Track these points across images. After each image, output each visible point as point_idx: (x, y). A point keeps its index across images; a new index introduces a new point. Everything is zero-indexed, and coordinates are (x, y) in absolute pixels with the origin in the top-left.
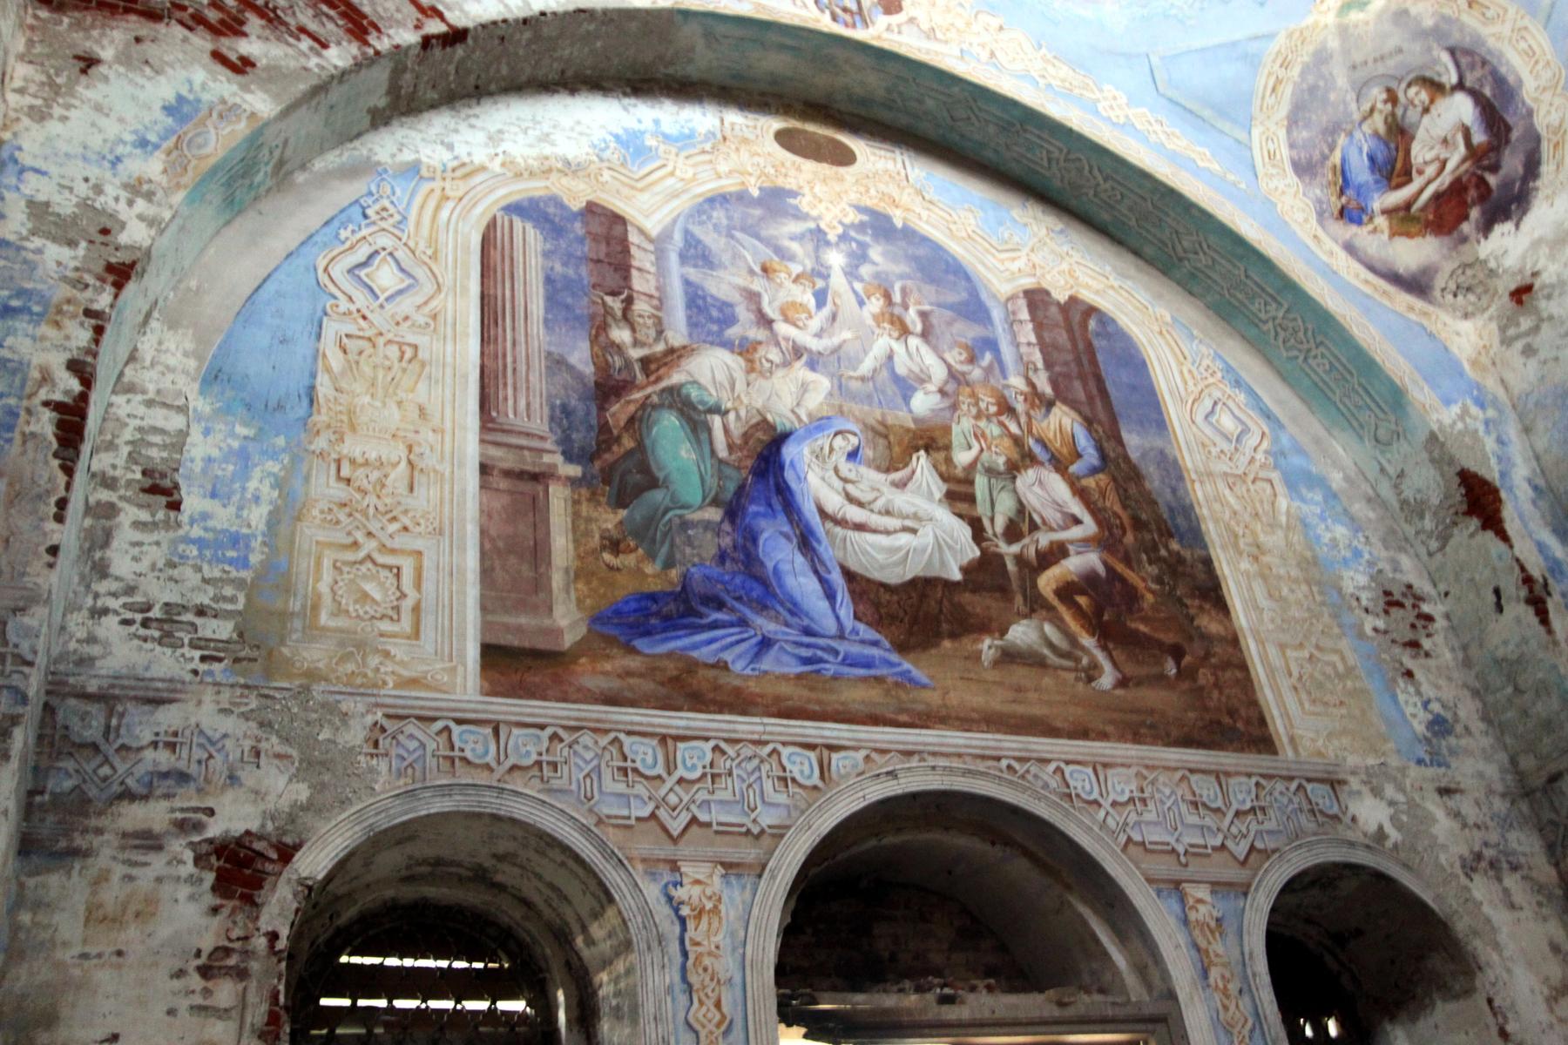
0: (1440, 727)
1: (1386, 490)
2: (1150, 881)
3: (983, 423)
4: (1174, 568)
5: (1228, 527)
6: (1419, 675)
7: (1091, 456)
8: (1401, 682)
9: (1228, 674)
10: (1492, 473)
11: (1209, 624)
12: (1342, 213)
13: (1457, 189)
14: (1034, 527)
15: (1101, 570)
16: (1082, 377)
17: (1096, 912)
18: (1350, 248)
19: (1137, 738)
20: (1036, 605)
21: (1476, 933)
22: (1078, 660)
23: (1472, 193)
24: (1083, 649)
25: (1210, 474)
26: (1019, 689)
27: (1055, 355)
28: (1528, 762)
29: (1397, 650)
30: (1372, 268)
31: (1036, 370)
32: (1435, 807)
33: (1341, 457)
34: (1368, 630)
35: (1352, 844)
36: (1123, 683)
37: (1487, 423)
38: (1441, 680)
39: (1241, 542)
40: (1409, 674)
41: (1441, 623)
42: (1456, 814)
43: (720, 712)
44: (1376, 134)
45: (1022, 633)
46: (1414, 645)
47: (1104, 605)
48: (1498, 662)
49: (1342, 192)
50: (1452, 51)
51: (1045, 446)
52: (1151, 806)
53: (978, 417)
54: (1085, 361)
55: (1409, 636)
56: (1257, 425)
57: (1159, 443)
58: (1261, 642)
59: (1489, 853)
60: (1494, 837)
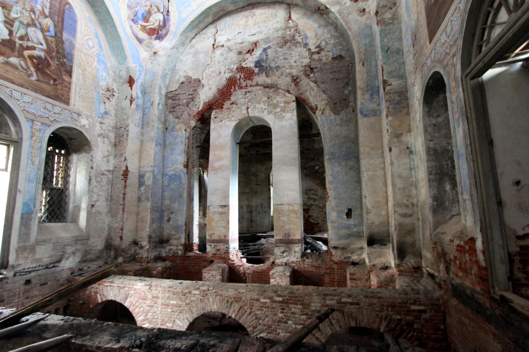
0: (106, 113)
1: (117, 72)
2: (26, 118)
3: (24, 11)
4: (63, 64)
5: (80, 62)
6: (107, 104)
7: (52, 33)
8: (102, 103)
9: (65, 89)
10: (135, 78)
11: (66, 78)
12: (133, 20)
13: (154, 30)
14: (28, 40)
15: (43, 57)
16: (59, 16)
17: (10, 119)
18: (131, 27)
19: (36, 91)
20: (21, 56)
21: (94, 145)
22: (28, 72)
23: (156, 32)
24: (30, 70)
25: (81, 51)
26: (7, 71)
27: (53, 7)
28: (118, 124)
29: (105, 98)
30: (133, 33)
31: (46, 7)
32: (98, 125)
33: (111, 61)
34: (101, 93)
35: (77, 125)
36: (38, 80)
37: (139, 70)
38: (111, 106)
39: (82, 67)
40: (105, 103)
41: (116, 97)
42: (101, 127)
43: (514, 34)
44: (145, 10)
45: (13, 60)
46: (109, 99)
47: (41, 65)
48: (122, 107)
49: (134, 16)
50: (164, 6)
51: (40, 25)
52: (33, 105)
53: (24, 9)
54: (61, 13)
55: (109, 97)
56: (97, 47)
57: (72, 39)
58: (76, 86)
59: (104, 134)
60: (106, 132)
